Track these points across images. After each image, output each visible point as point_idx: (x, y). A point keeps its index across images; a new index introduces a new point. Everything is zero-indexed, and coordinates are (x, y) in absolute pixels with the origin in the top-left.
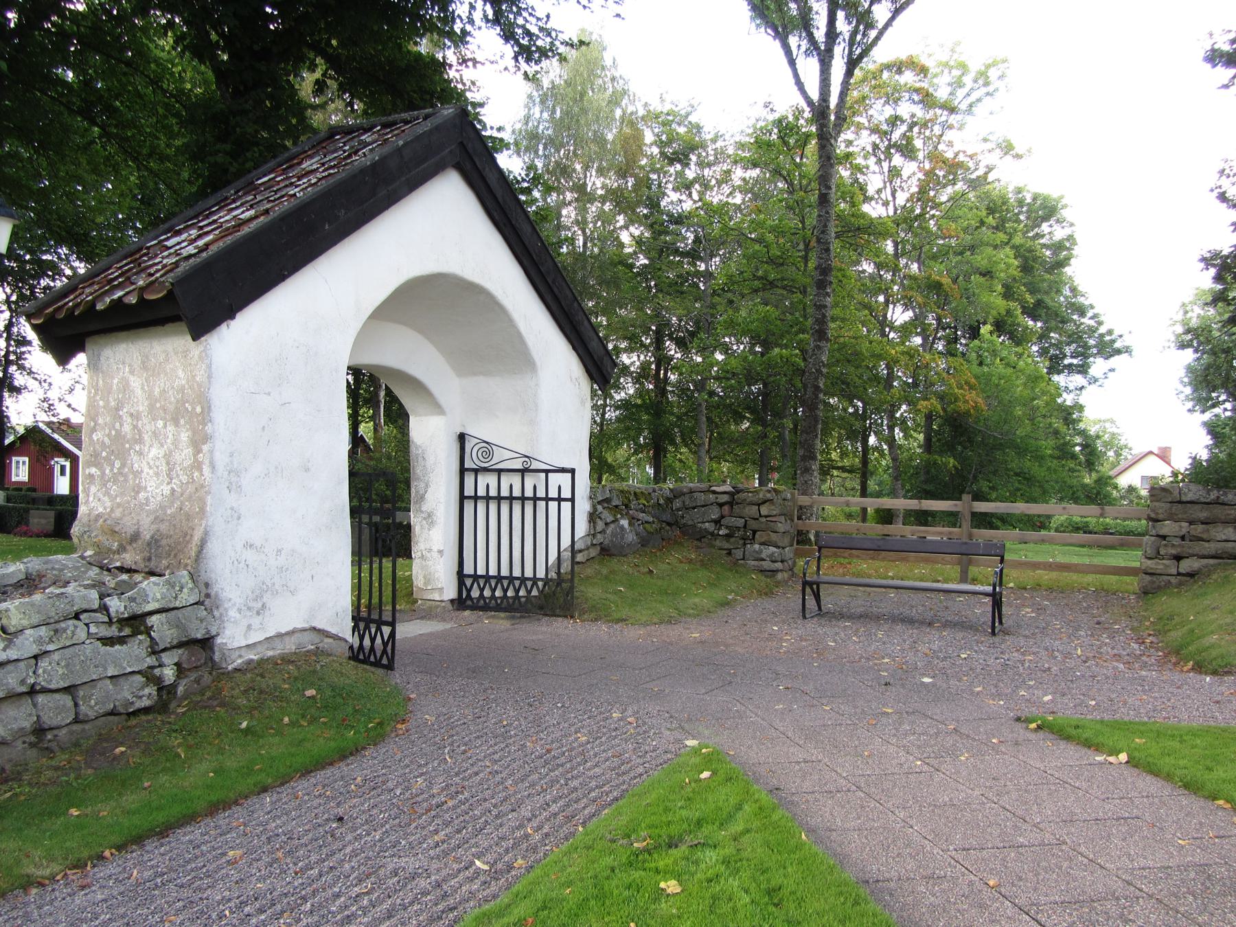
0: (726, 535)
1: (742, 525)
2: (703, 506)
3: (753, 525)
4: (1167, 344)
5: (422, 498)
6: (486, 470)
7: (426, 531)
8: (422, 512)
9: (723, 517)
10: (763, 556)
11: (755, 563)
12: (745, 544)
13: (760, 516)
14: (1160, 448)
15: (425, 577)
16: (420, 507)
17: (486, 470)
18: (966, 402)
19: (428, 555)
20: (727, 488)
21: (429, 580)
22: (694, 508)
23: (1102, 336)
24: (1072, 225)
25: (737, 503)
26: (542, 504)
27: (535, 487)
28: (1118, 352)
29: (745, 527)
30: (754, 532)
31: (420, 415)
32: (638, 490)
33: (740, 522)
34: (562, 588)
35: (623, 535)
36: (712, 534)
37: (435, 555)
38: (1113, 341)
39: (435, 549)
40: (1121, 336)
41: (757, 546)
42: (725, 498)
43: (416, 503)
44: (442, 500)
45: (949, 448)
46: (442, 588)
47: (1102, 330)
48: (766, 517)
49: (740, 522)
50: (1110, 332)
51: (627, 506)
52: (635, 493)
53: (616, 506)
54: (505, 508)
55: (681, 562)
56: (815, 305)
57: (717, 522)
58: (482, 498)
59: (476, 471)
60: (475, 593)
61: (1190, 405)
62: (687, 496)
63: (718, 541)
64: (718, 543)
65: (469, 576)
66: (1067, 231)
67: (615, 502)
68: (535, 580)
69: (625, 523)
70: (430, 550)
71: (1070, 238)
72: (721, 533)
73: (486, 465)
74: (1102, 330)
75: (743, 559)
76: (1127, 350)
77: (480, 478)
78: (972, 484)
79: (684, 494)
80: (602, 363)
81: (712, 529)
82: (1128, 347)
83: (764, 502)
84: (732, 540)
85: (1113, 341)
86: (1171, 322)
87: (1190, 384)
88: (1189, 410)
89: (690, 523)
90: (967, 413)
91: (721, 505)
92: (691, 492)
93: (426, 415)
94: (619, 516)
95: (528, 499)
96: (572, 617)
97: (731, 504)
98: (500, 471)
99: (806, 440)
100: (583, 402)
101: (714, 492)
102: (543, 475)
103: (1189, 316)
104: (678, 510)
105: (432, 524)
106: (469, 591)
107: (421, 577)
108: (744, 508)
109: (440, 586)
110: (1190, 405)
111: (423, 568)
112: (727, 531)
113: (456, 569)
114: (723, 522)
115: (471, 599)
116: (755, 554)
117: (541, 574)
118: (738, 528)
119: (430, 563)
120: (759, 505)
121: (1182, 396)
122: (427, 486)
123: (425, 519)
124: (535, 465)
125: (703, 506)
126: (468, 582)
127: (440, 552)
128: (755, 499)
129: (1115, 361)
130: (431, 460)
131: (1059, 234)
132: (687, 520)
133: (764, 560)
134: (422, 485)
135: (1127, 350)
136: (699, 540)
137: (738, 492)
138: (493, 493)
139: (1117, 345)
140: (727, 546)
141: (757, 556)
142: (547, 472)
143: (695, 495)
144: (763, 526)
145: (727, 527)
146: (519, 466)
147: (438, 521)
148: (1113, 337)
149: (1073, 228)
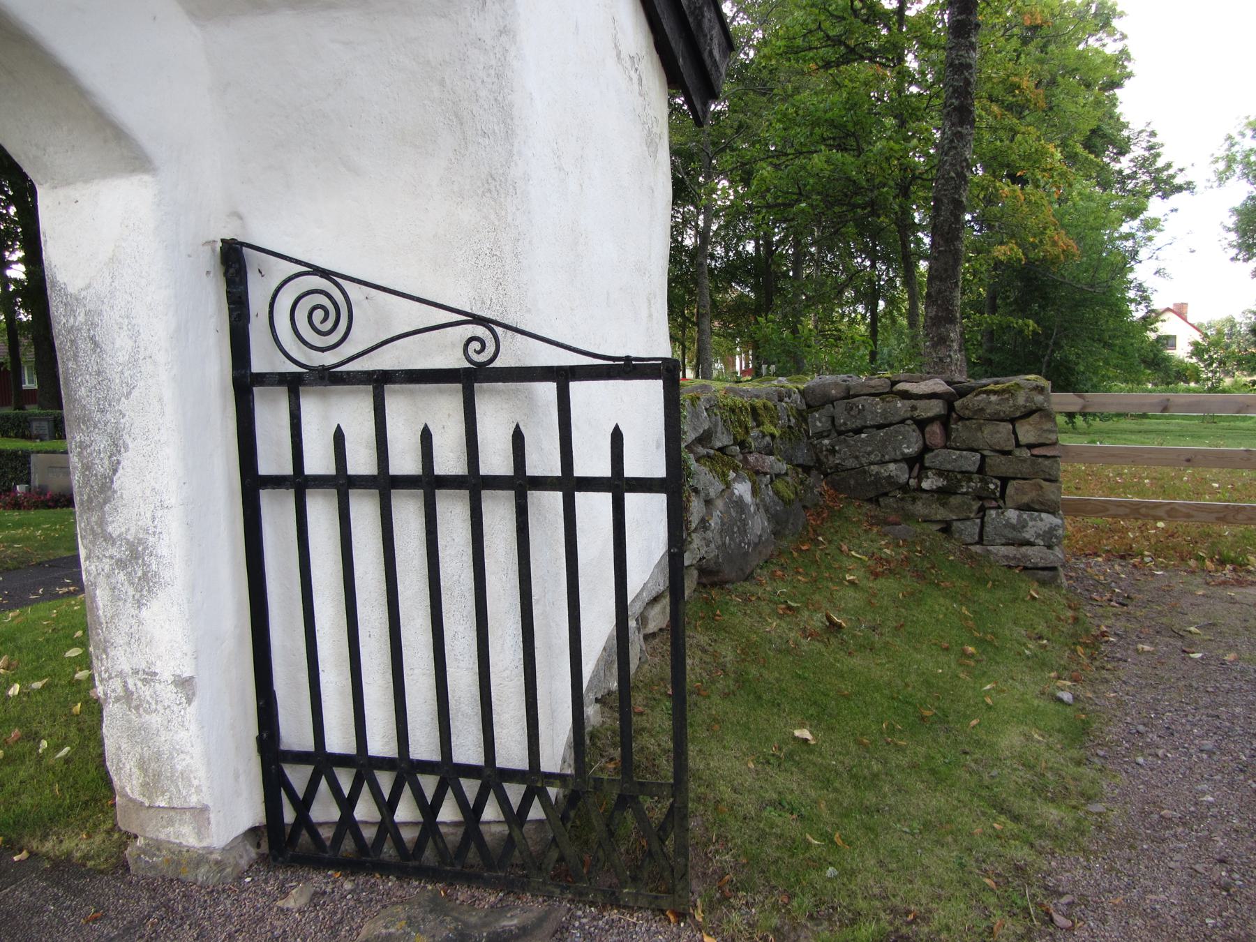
0: (940, 491)
1: (974, 468)
2: (880, 427)
3: (999, 465)
4: (1209, 184)
5: (105, 488)
6: (329, 378)
7: (129, 609)
8: (109, 539)
9: (926, 449)
10: (1029, 534)
11: (1011, 551)
12: (982, 510)
13: (1018, 445)
14: (1175, 305)
15: (142, 765)
16: (102, 522)
17: (329, 378)
18: (1055, 244)
19: (146, 692)
20: (937, 385)
21: (157, 775)
22: (858, 431)
23: (1159, 171)
24: (1124, 37)
25: (961, 418)
26: (548, 504)
27: (518, 438)
28: (1179, 189)
29: (981, 470)
30: (1005, 481)
31: (67, 182)
32: (758, 403)
33: (971, 461)
34: (641, 816)
35: (744, 523)
36: (905, 488)
37: (168, 693)
38: (1173, 177)
39: (166, 671)
40: (1181, 170)
41: (1012, 514)
42: (936, 407)
43: (89, 507)
44: (172, 499)
45: (1022, 308)
46: (204, 809)
47: (1160, 163)
48: (1030, 446)
49: (971, 461)
50: (1169, 166)
51: (742, 444)
52: (754, 410)
53: (722, 450)
54: (408, 512)
55: (876, 575)
56: (951, 65)
57: (916, 462)
58: (320, 482)
59: (294, 384)
60: (325, 811)
61: (1233, 252)
62: (841, 406)
63: (919, 503)
64: (919, 508)
65: (300, 758)
66: (1119, 46)
67: (722, 439)
68: (533, 778)
69: (743, 489)
70: (150, 677)
71: (1124, 54)
72: (926, 485)
73: (329, 359)
74: (1160, 163)
75: (980, 541)
76: (1189, 186)
77: (311, 408)
78: (1053, 351)
79: (832, 401)
80: (699, 24)
81: (903, 478)
82: (1189, 183)
83: (1028, 414)
84: (954, 500)
85: (1173, 177)
86: (1212, 159)
87: (1236, 230)
88: (1232, 259)
89: (851, 463)
90: (1054, 261)
91: (922, 424)
92: (848, 395)
93: (86, 178)
94: (732, 475)
95: (496, 483)
96: (681, 916)
97: (944, 420)
98: (380, 381)
99: (939, 292)
100: (650, 143)
101: (905, 395)
102: (547, 391)
103: (1234, 149)
104: (820, 435)
105: (146, 584)
106: (303, 806)
107: (130, 765)
108: (980, 428)
109: (194, 800)
110: (1233, 252)
111: (139, 734)
112: (941, 482)
113: (251, 728)
114: (929, 459)
115: (312, 828)
116: (1007, 532)
117: (554, 756)
118: (967, 475)
119: (155, 720)
120: (1013, 421)
121: (1225, 243)
122: (117, 447)
123: (121, 564)
124: (515, 353)
125: (880, 427)
126: (298, 777)
127: (185, 684)
128: (1006, 408)
129: (1176, 199)
130: (119, 346)
131: (1112, 48)
132: (844, 456)
133: (1031, 544)
134: (101, 443)
135: (1189, 186)
136: (875, 501)
137: (962, 393)
138: (361, 462)
139: (1179, 180)
140: (942, 514)
141: (1011, 534)
142: (562, 376)
143: (860, 402)
144: (1025, 468)
145: (940, 473)
146: (453, 360)
147: (166, 575)
148: (1171, 171)
149: (1125, 42)
